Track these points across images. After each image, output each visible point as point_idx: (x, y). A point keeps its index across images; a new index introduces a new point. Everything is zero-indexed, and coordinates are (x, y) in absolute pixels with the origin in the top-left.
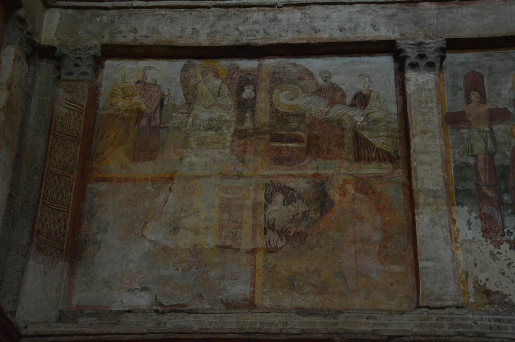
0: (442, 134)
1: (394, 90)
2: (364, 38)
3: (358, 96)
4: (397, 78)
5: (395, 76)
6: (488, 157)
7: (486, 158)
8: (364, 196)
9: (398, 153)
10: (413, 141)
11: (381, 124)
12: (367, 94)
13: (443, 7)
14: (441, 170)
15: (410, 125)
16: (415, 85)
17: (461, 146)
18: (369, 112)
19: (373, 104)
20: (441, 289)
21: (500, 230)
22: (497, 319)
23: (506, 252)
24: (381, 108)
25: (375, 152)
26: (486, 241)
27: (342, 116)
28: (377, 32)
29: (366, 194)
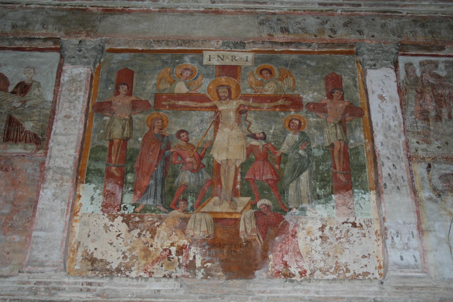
1: (54, 81)
5: (58, 69)
6: (122, 141)
11: (35, 110)
16: (69, 77)
20: (46, 256)
26: (103, 215)
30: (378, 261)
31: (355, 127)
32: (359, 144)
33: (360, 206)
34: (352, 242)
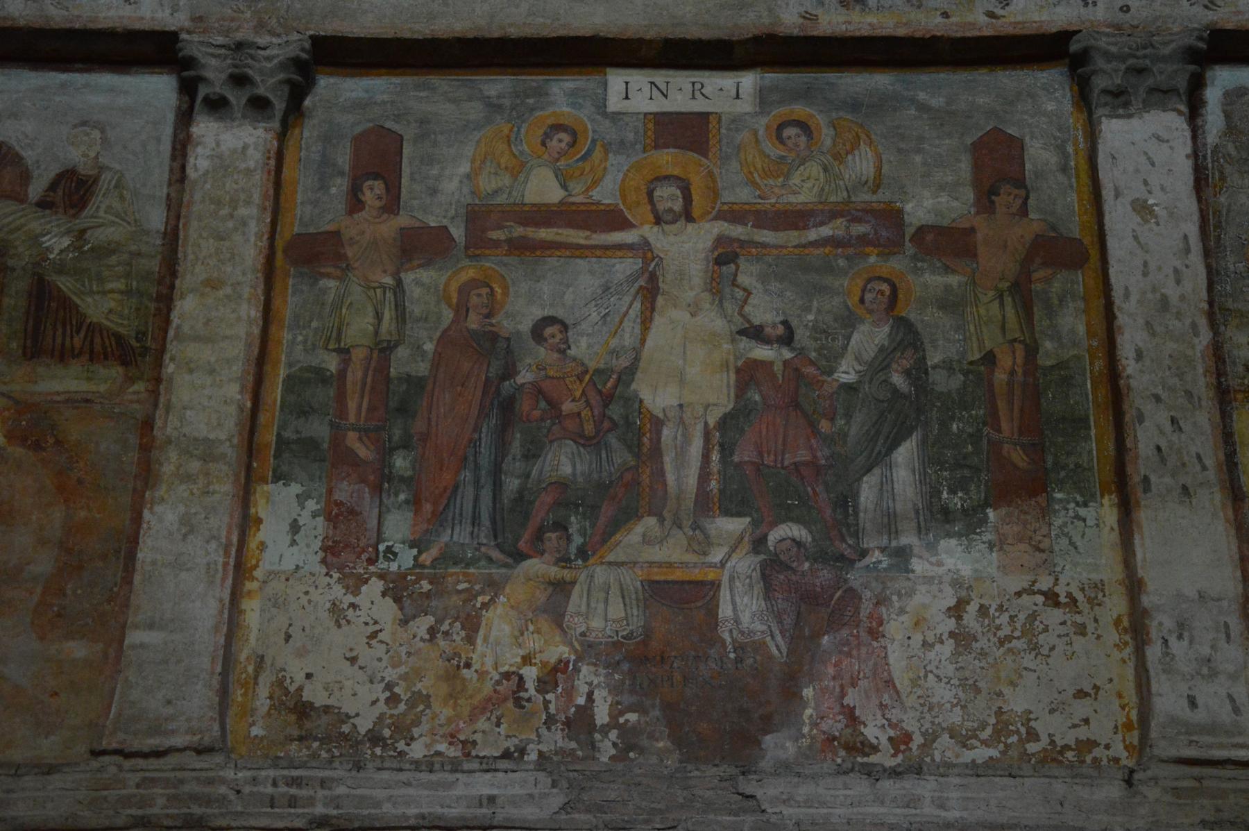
1: (167, 169)
7: (371, 358)
8: (31, 454)
10: (178, 308)
11: (113, 259)
12: (90, 176)
17: (314, 324)
18: (86, 225)
19: (102, 204)
20: (169, 702)
21: (368, 546)
22: (292, 778)
23: (372, 603)
25: (82, 334)
26: (327, 574)
27: (12, 232)
29: (37, 446)
30: (1123, 707)
31: (1061, 301)
32: (1071, 353)
33: (1072, 543)
34: (1045, 651)
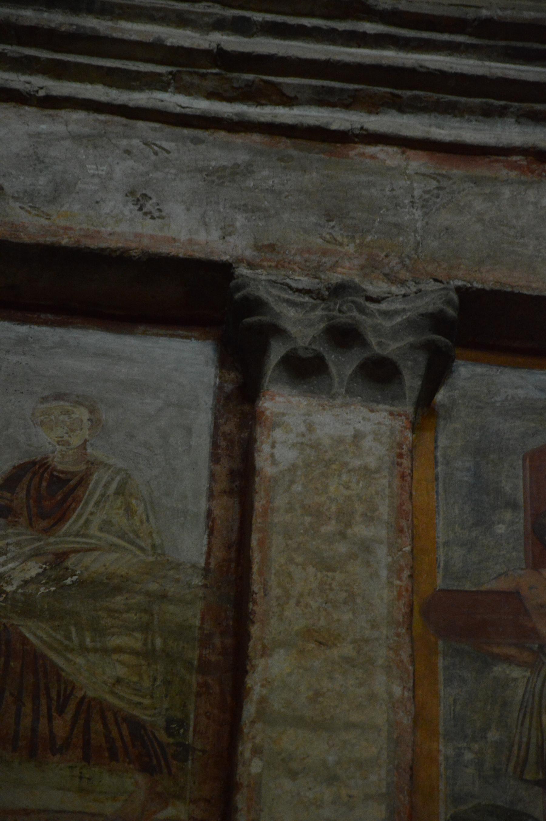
0: (405, 656)
1: (205, 473)
2: (86, 236)
3: (29, 476)
4: (227, 429)
5: (216, 418)
9: (186, 730)
10: (260, 669)
11: (119, 601)
12: (74, 474)
13: (457, 172)
14: (383, 808)
15: (255, 603)
17: (493, 735)
24: (131, 535)
28: (149, 221)
